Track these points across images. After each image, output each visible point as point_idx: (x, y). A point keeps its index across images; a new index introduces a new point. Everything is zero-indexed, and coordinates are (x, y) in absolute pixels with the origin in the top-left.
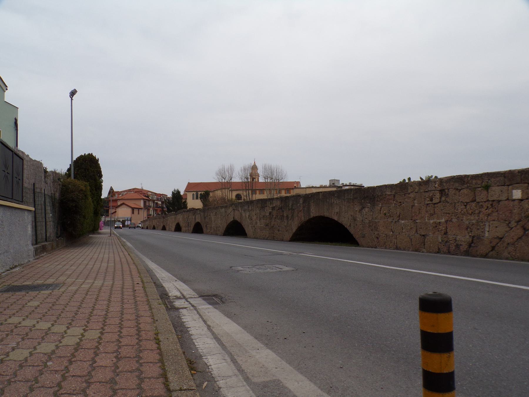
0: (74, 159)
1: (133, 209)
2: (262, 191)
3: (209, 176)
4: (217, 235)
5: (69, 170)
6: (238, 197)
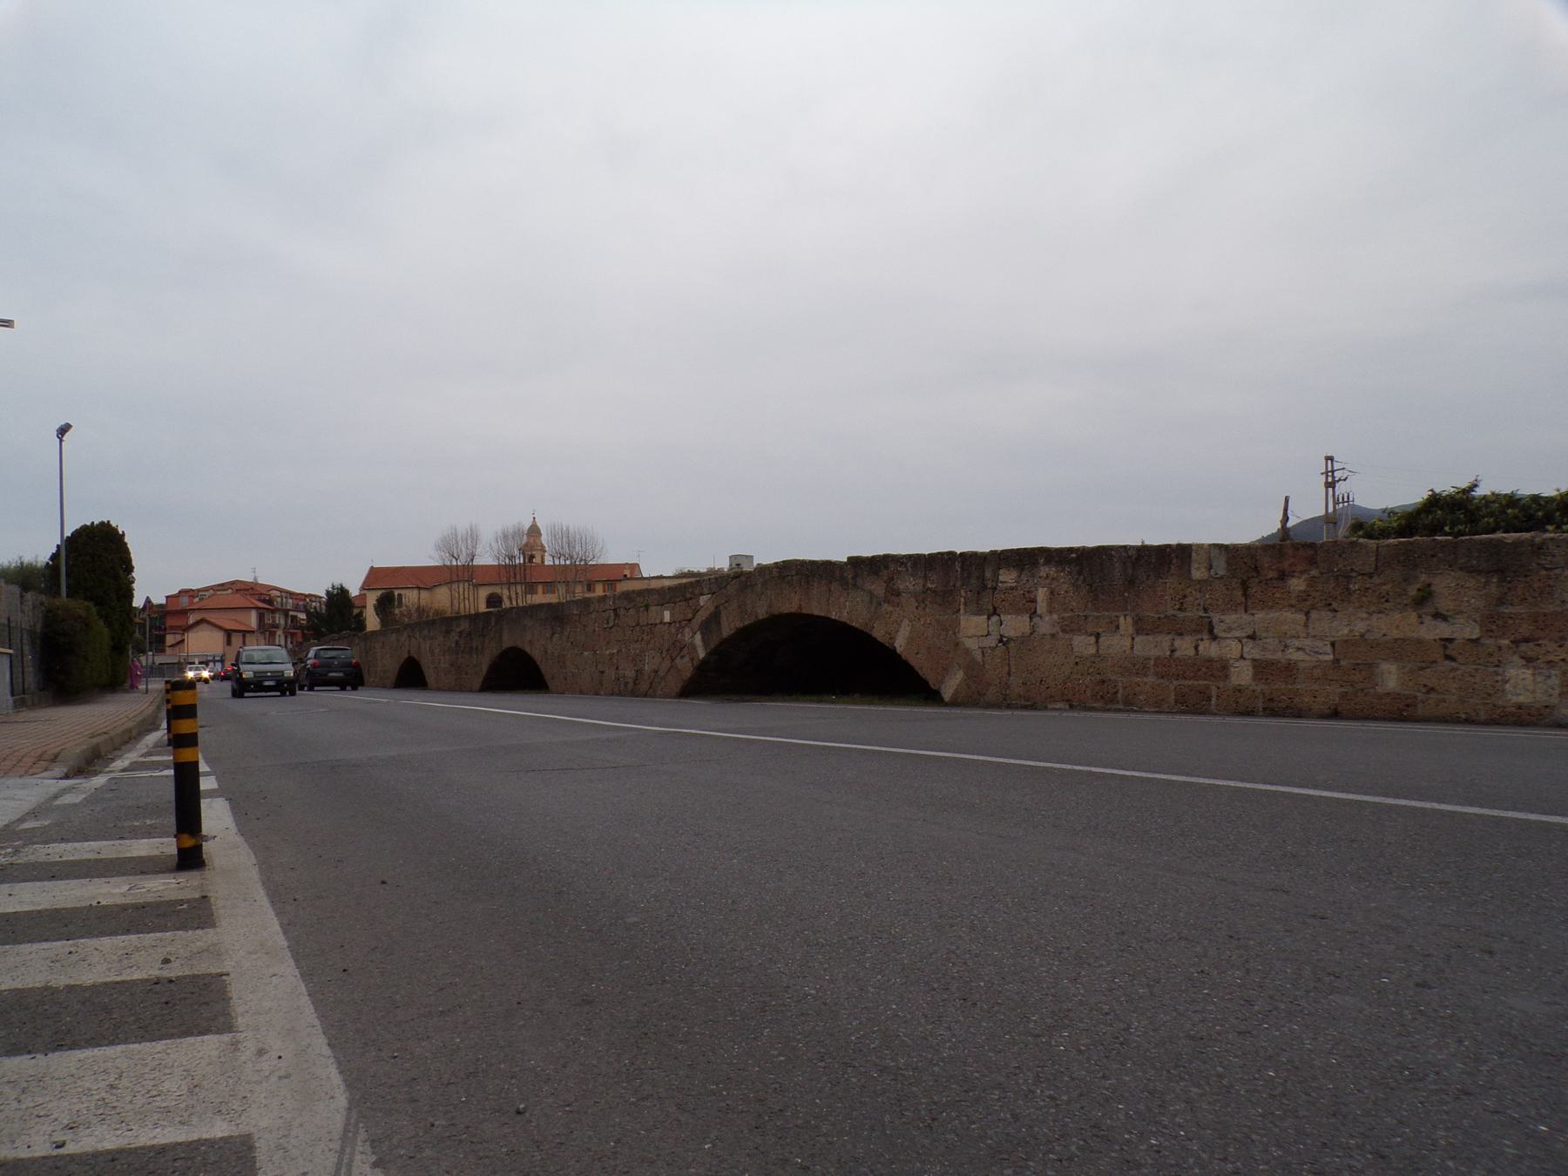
0: (68, 533)
1: (229, 633)
2: (549, 586)
4: (384, 687)
5: (55, 557)
6: (493, 600)
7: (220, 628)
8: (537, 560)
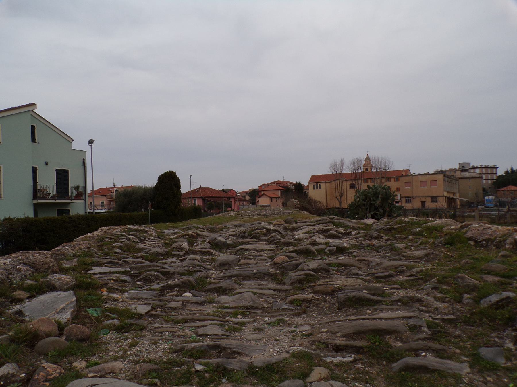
1: (271, 198)
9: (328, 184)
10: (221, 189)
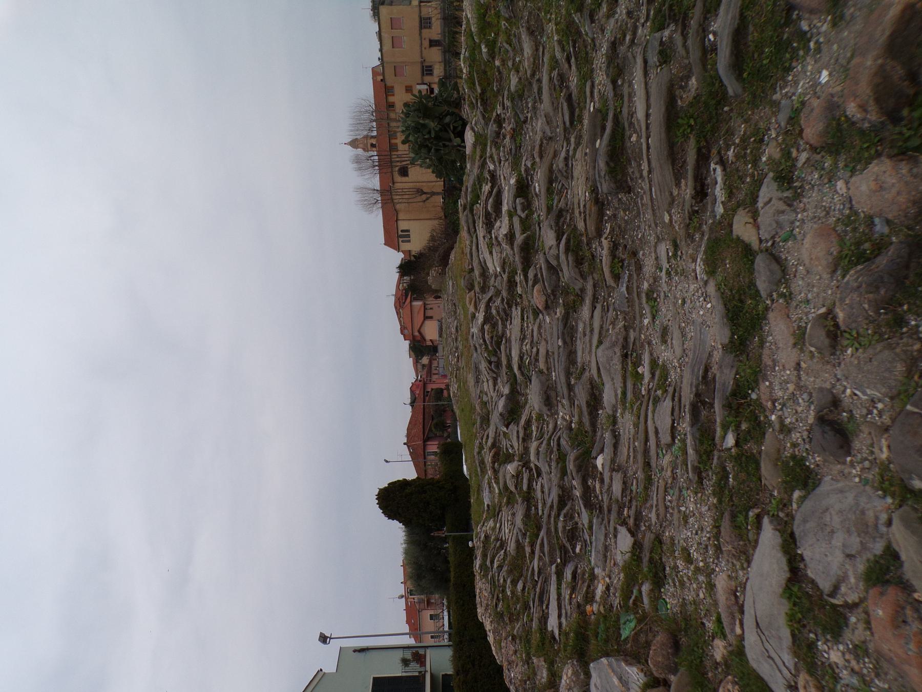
1: (426, 318)
2: (392, 135)
3: (374, 222)
7: (423, 323)
8: (374, 141)
9: (401, 216)
10: (409, 409)
